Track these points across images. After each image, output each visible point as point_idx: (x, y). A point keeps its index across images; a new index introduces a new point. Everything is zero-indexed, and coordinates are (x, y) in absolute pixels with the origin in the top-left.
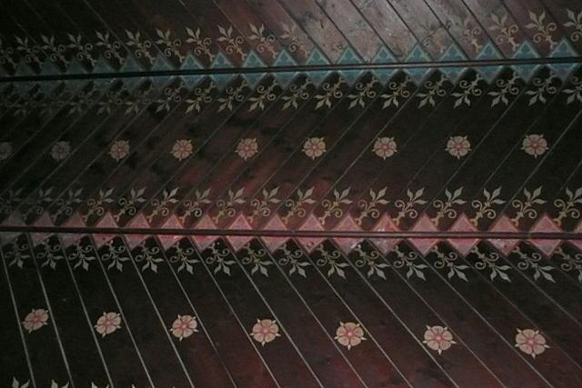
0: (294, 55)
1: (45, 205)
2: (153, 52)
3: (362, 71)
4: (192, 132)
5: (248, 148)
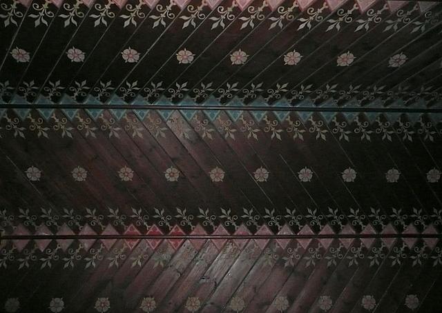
0: (205, 117)
1: (422, 19)
2: (309, 124)
3: (203, 105)
4: (284, 69)
5: (239, 57)
